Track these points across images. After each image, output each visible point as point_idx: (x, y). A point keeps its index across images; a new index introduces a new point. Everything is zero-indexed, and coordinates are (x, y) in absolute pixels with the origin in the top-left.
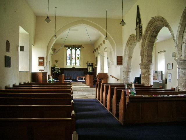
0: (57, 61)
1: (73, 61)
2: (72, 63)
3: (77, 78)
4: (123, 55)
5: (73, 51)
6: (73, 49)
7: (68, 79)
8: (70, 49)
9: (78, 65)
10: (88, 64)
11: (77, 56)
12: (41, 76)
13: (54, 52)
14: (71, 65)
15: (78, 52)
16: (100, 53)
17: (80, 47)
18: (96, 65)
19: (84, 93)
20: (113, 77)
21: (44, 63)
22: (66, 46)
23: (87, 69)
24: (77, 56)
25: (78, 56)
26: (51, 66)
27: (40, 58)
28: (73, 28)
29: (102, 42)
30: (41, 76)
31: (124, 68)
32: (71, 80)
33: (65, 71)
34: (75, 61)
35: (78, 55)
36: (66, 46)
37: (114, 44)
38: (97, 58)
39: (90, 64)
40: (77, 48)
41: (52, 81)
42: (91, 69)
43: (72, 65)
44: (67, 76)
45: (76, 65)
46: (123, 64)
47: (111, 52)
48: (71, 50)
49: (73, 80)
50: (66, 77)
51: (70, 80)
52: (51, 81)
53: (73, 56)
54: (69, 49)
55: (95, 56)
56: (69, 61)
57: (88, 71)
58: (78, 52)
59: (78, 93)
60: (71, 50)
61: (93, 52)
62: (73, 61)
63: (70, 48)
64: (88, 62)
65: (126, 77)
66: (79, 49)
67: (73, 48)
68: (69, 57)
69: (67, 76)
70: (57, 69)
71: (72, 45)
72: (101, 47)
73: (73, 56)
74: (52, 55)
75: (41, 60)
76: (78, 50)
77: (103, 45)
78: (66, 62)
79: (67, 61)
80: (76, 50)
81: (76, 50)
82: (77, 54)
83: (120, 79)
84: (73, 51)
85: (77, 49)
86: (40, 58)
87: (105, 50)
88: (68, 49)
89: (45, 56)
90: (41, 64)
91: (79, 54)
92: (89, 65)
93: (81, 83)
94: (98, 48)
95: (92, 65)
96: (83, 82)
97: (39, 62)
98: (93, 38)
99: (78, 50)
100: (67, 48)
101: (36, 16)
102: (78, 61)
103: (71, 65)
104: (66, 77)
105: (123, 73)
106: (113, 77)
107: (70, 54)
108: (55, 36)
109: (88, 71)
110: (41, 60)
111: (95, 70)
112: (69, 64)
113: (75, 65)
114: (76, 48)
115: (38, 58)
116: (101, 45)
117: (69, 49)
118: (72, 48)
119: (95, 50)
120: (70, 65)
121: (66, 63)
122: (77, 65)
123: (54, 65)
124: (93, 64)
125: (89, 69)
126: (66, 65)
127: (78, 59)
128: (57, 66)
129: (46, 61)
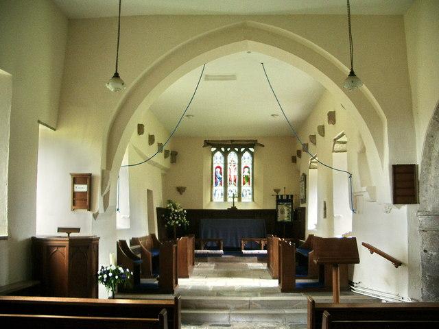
0: (181, 190)
1: (233, 189)
2: (230, 194)
3: (241, 244)
4: (418, 160)
5: (233, 157)
6: (233, 153)
7: (215, 245)
8: (221, 151)
9: (247, 203)
10: (277, 196)
11: (246, 173)
12: (63, 254)
13: (173, 161)
14: (225, 200)
15: (246, 160)
16: (343, 139)
17: (252, 146)
18: (304, 200)
19: (256, 320)
20: (373, 250)
21: (94, 199)
22: (208, 143)
23: (273, 213)
24: (246, 173)
25: (247, 174)
26: (157, 203)
27: (77, 179)
28: (213, 67)
29: (315, 131)
30: (63, 254)
31: (423, 212)
32: (222, 251)
33: (203, 221)
34: (236, 188)
35: (247, 170)
36: (208, 143)
37: (379, 118)
38: (305, 176)
39: (285, 198)
40: (242, 150)
41: (114, 276)
42: (286, 214)
43: (230, 200)
44: (212, 237)
45: (240, 200)
46: (421, 199)
47: (363, 151)
48: (225, 154)
49: (228, 250)
50: (209, 240)
51: (218, 252)
52: (110, 274)
53: (233, 173)
54: (219, 152)
55: (299, 172)
56: (219, 189)
57: (279, 220)
58: (246, 160)
59: (233, 318)
60: (225, 154)
61: (294, 160)
62: (233, 189)
63: (223, 149)
64: (277, 191)
65: (434, 254)
66: (250, 152)
67: (232, 149)
68: (219, 175)
69: (209, 237)
70: (176, 213)
71: (227, 141)
72: (319, 137)
73: (233, 173)
74: (167, 170)
75: (82, 188)
76: (247, 155)
77: (329, 128)
78: (211, 191)
79: (215, 188)
80: (240, 154)
81: (240, 154)
82: (243, 166)
83: (406, 261)
84: (233, 157)
85: (244, 152)
86: (77, 179)
87: (337, 147)
88: (215, 152)
89: (95, 169)
90: (82, 201)
91: (250, 166)
92: (279, 200)
93: (253, 262)
94: (311, 145)
95: (288, 200)
96: (261, 258)
97: (74, 194)
98: (291, 111)
99: (247, 155)
100: (213, 149)
101: (69, 20)
102: (247, 188)
103: (225, 200)
104: (209, 240)
105: (420, 239)
106: (373, 250)
107: (222, 166)
108: (116, 75)
109: (279, 220)
110: (82, 188)
111: (299, 215)
112: (217, 200)
113: (236, 200)
114: (239, 150)
115: (70, 180)
116: (322, 130)
117: (219, 152)
118: (229, 149)
119: (298, 151)
120: (222, 200)
121: (210, 196)
122: (243, 200)
123: (169, 202)
124: (292, 196)
125: (282, 212)
126: (211, 200)
127: (248, 181)
128: (178, 205)
129: (102, 191)
